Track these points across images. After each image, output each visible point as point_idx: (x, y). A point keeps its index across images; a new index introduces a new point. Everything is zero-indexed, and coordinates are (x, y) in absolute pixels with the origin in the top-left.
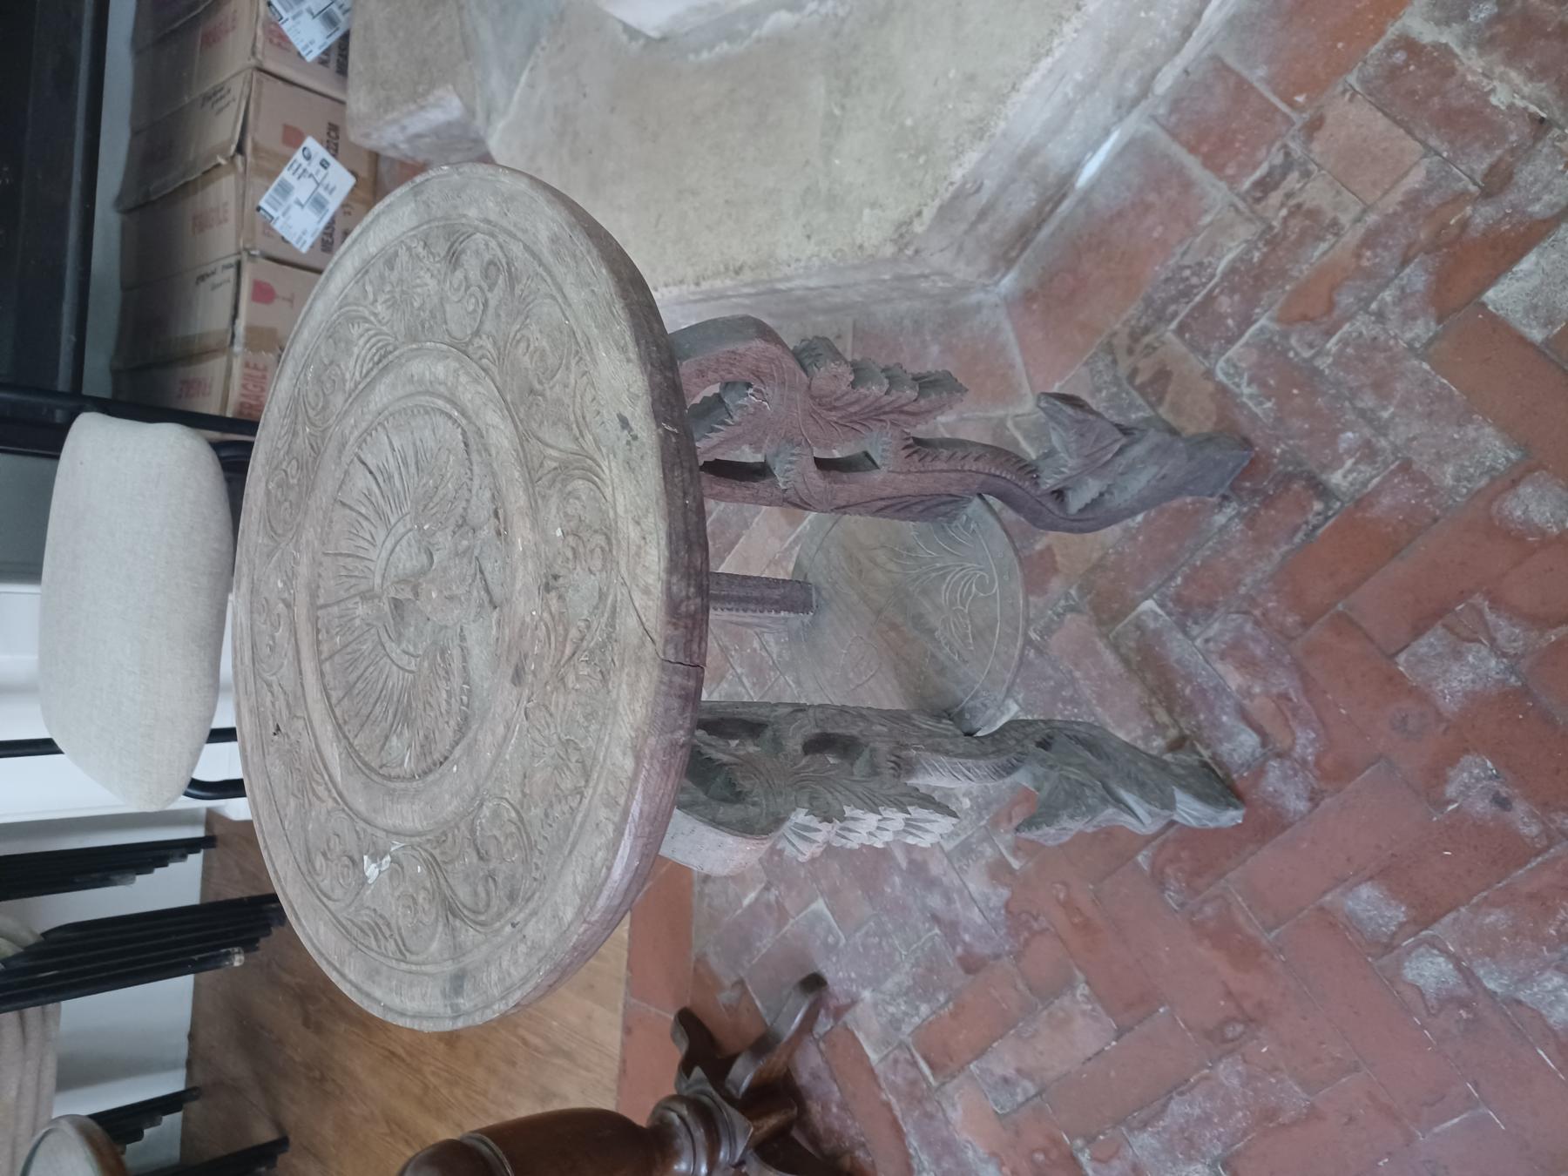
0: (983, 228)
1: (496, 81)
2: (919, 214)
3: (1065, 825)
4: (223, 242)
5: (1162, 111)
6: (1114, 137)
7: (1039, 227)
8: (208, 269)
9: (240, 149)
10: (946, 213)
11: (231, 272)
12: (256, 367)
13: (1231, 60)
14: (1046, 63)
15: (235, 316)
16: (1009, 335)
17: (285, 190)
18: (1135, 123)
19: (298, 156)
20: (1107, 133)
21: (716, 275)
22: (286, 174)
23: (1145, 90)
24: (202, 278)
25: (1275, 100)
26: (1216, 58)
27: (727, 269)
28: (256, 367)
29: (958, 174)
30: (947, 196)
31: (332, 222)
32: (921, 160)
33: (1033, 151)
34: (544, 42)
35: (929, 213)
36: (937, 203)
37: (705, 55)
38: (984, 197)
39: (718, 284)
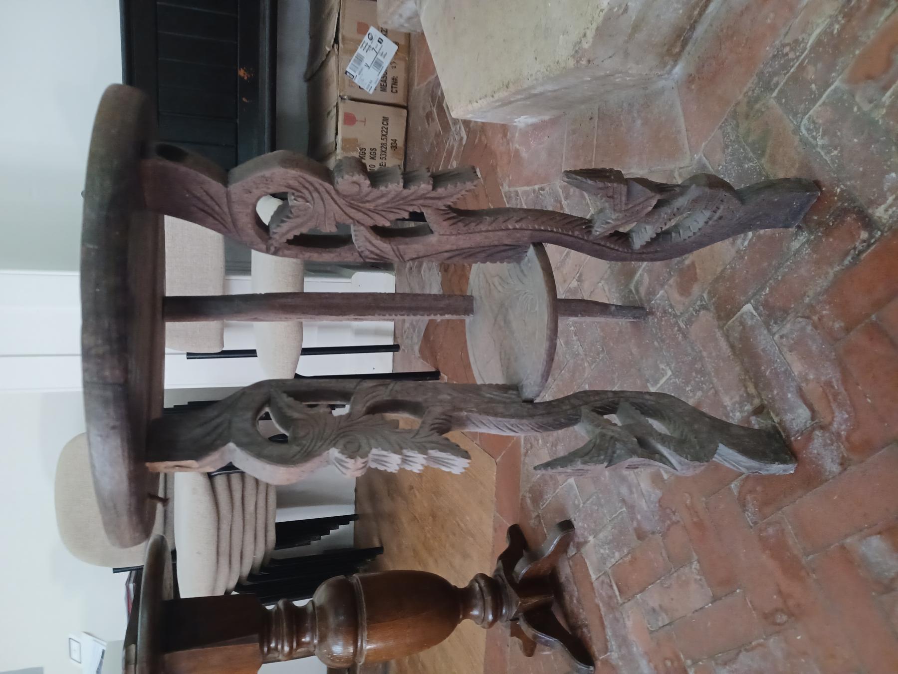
0: (641, 36)
2: (585, 35)
7: (693, 27)
17: (360, 59)
19: (366, 39)
22: (360, 51)
31: (386, 73)
35: (590, 34)
36: (594, 26)
38: (633, 14)
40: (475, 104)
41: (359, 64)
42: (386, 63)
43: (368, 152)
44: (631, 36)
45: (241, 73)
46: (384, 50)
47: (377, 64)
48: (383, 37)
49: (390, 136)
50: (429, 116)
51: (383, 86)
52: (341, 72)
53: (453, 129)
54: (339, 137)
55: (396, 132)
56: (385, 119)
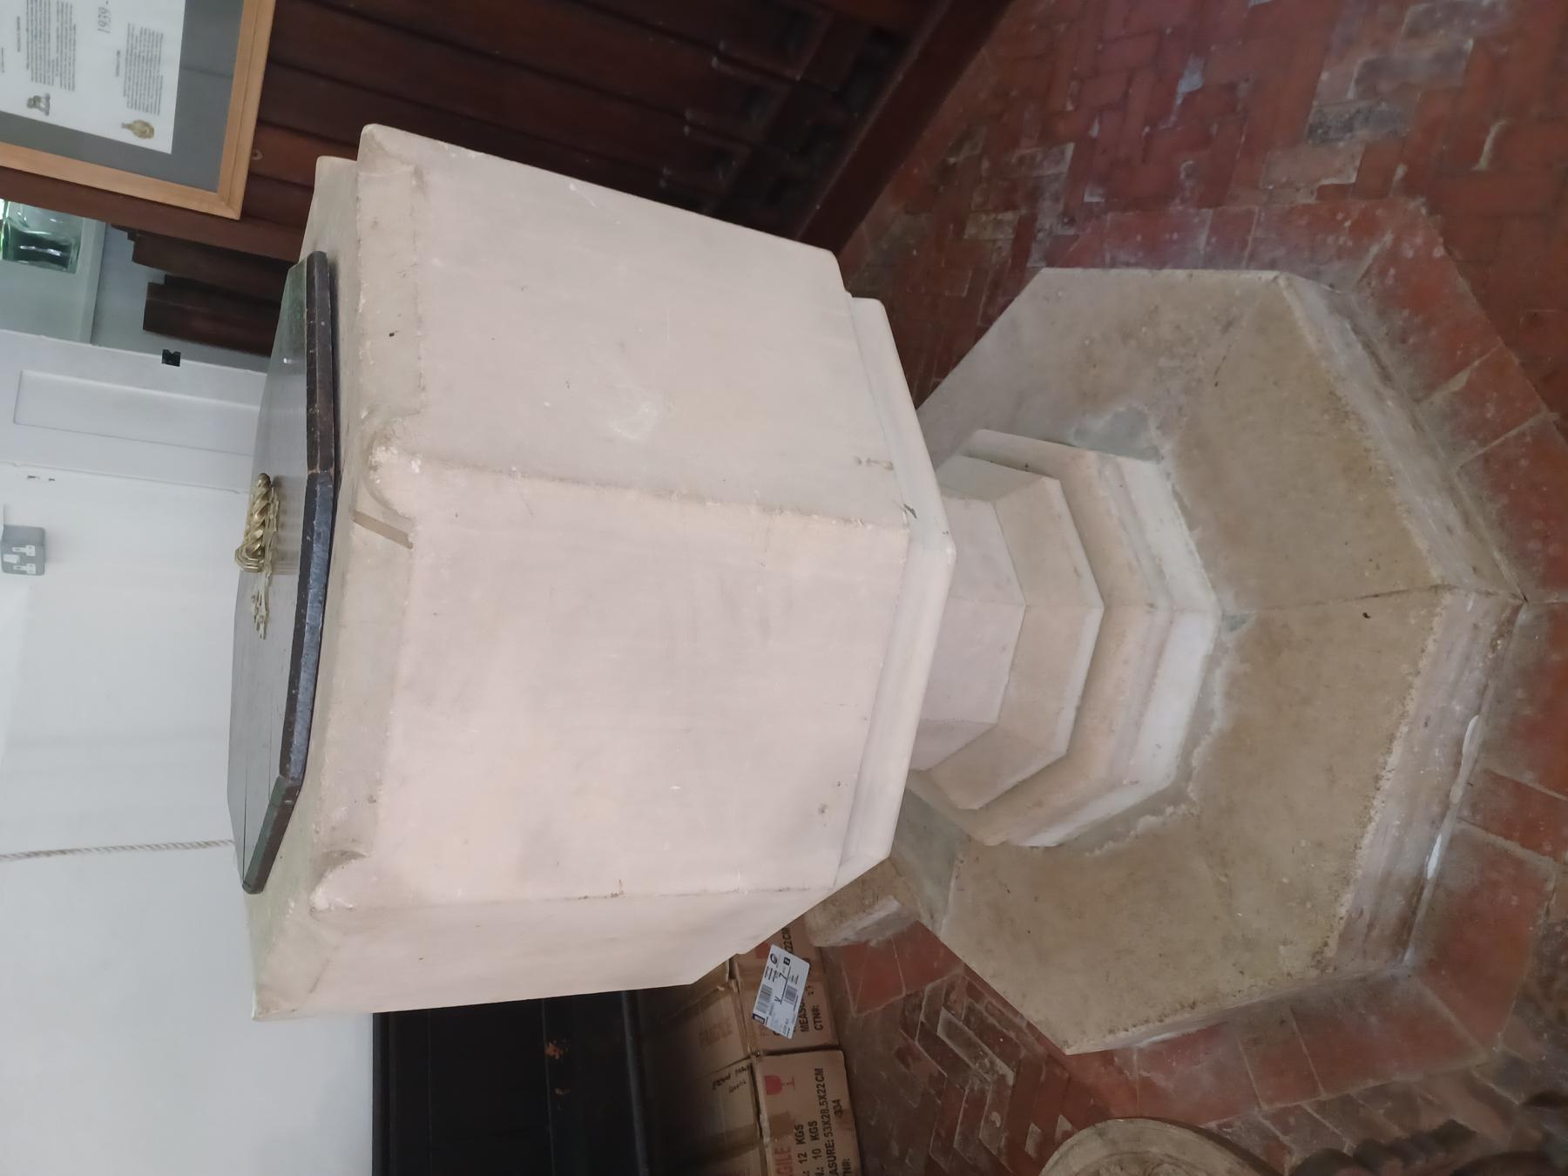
0: (1375, 933)
1: (930, 889)
2: (1326, 944)
3: (1448, 826)
4: (732, 1049)
5: (1466, 813)
6: (1439, 840)
7: (1414, 913)
8: (725, 1073)
9: (732, 976)
10: (1345, 938)
11: (745, 1076)
12: (782, 1152)
13: (1501, 771)
14: (1371, 827)
15: (758, 1113)
16: (1433, 999)
17: (767, 993)
18: (1448, 826)
19: (769, 963)
20: (1433, 841)
21: (1176, 1012)
22: (765, 981)
23: (1446, 805)
24: (718, 1083)
25: (1551, 793)
26: (1486, 771)
27: (1183, 1007)
28: (782, 1152)
29: (1343, 911)
30: (1341, 927)
31: (803, 1003)
32: (1309, 905)
33: (1388, 875)
34: (960, 857)
35: (1333, 943)
36: (1336, 933)
37: (1097, 852)
38: (1367, 916)
39: (1178, 1018)
40: (1122, 1034)
41: (768, 999)
42: (800, 992)
43: (806, 1129)
44: (1367, 935)
45: (551, 1050)
46: (794, 973)
47: (790, 994)
48: (789, 956)
49: (830, 1097)
50: (904, 1055)
51: (802, 1024)
52: (747, 1017)
53: (975, 1066)
54: (764, 1116)
55: (837, 1090)
56: (819, 1072)
